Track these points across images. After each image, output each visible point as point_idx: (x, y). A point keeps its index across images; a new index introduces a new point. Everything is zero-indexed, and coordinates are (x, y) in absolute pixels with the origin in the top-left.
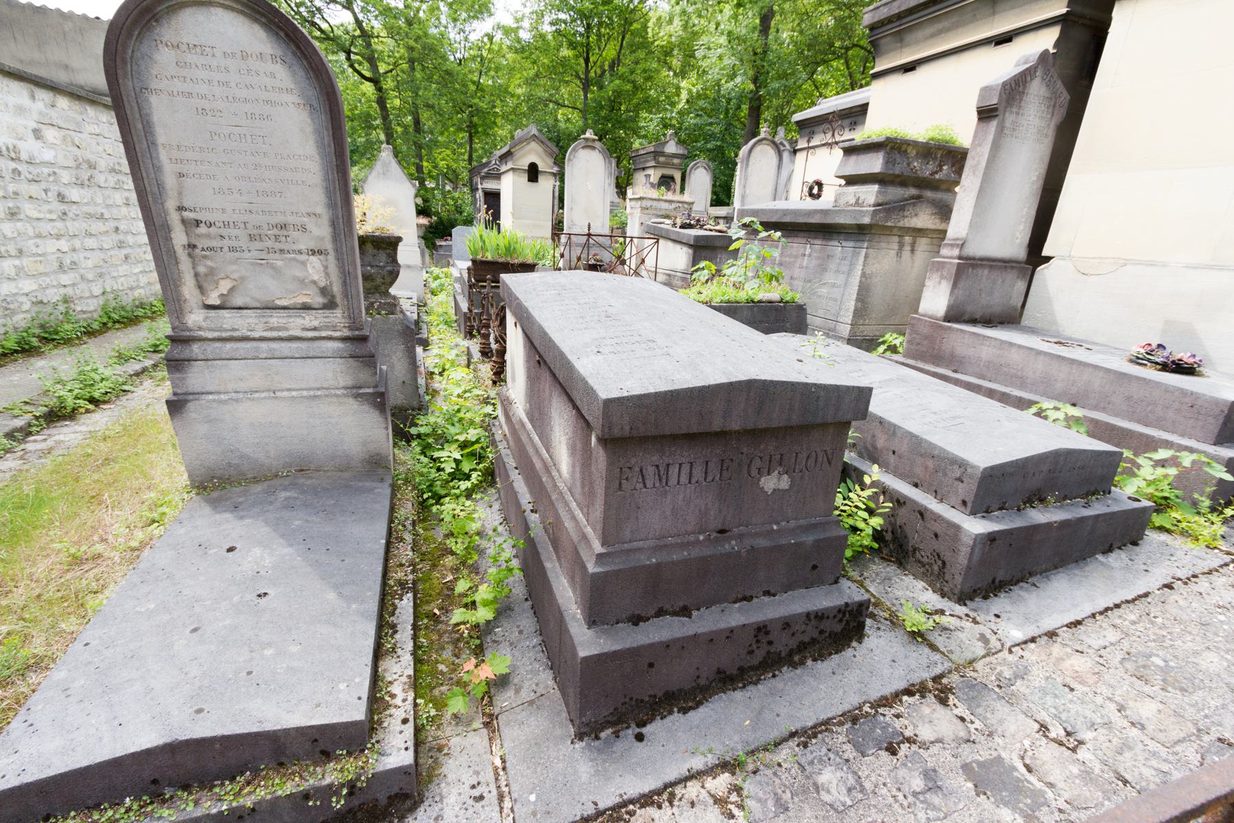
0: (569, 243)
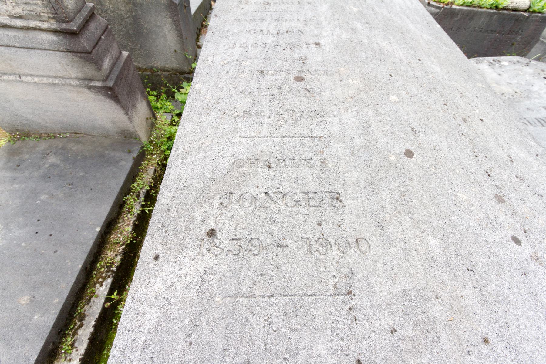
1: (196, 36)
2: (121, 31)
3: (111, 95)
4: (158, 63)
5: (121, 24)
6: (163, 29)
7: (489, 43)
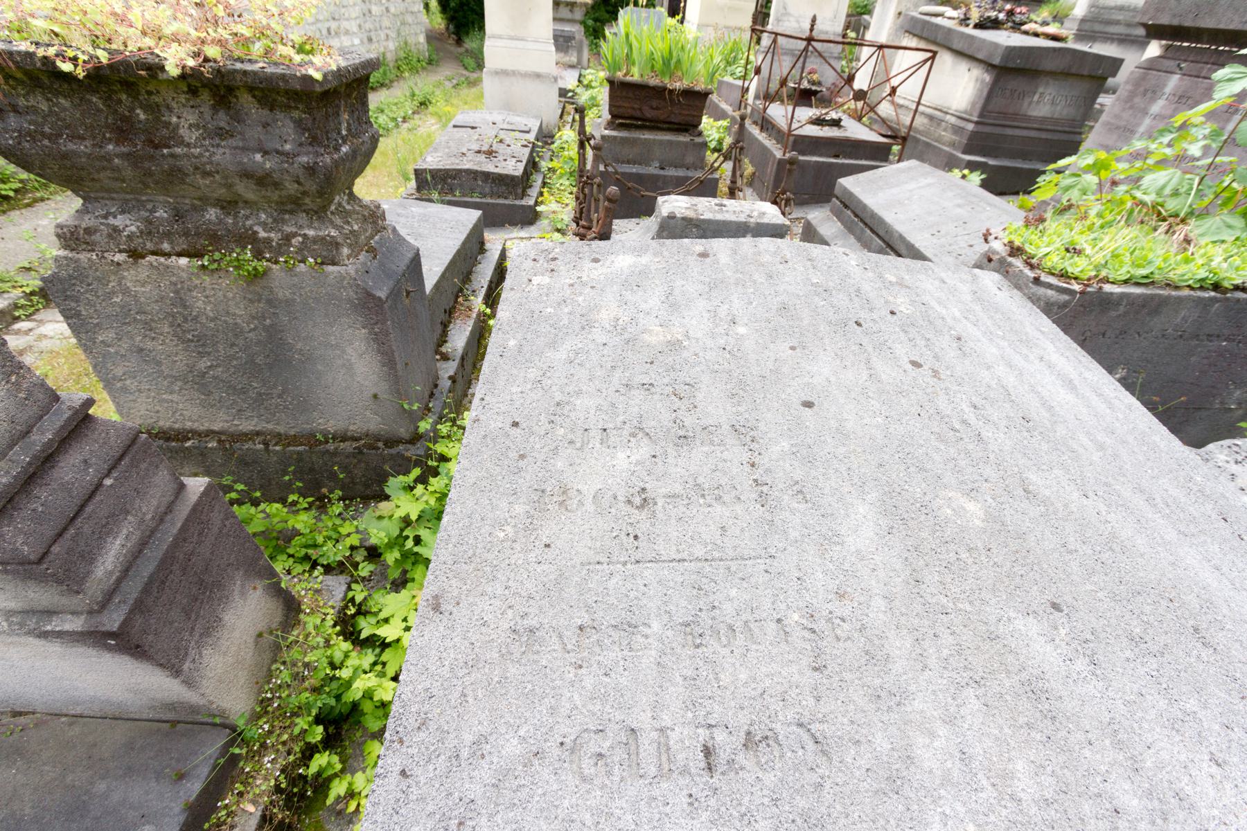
0: (773, 48)
1: (439, 329)
2: (233, 357)
3: (117, 645)
4: (330, 421)
5: (233, 345)
6: (344, 352)
7: (1205, 361)
